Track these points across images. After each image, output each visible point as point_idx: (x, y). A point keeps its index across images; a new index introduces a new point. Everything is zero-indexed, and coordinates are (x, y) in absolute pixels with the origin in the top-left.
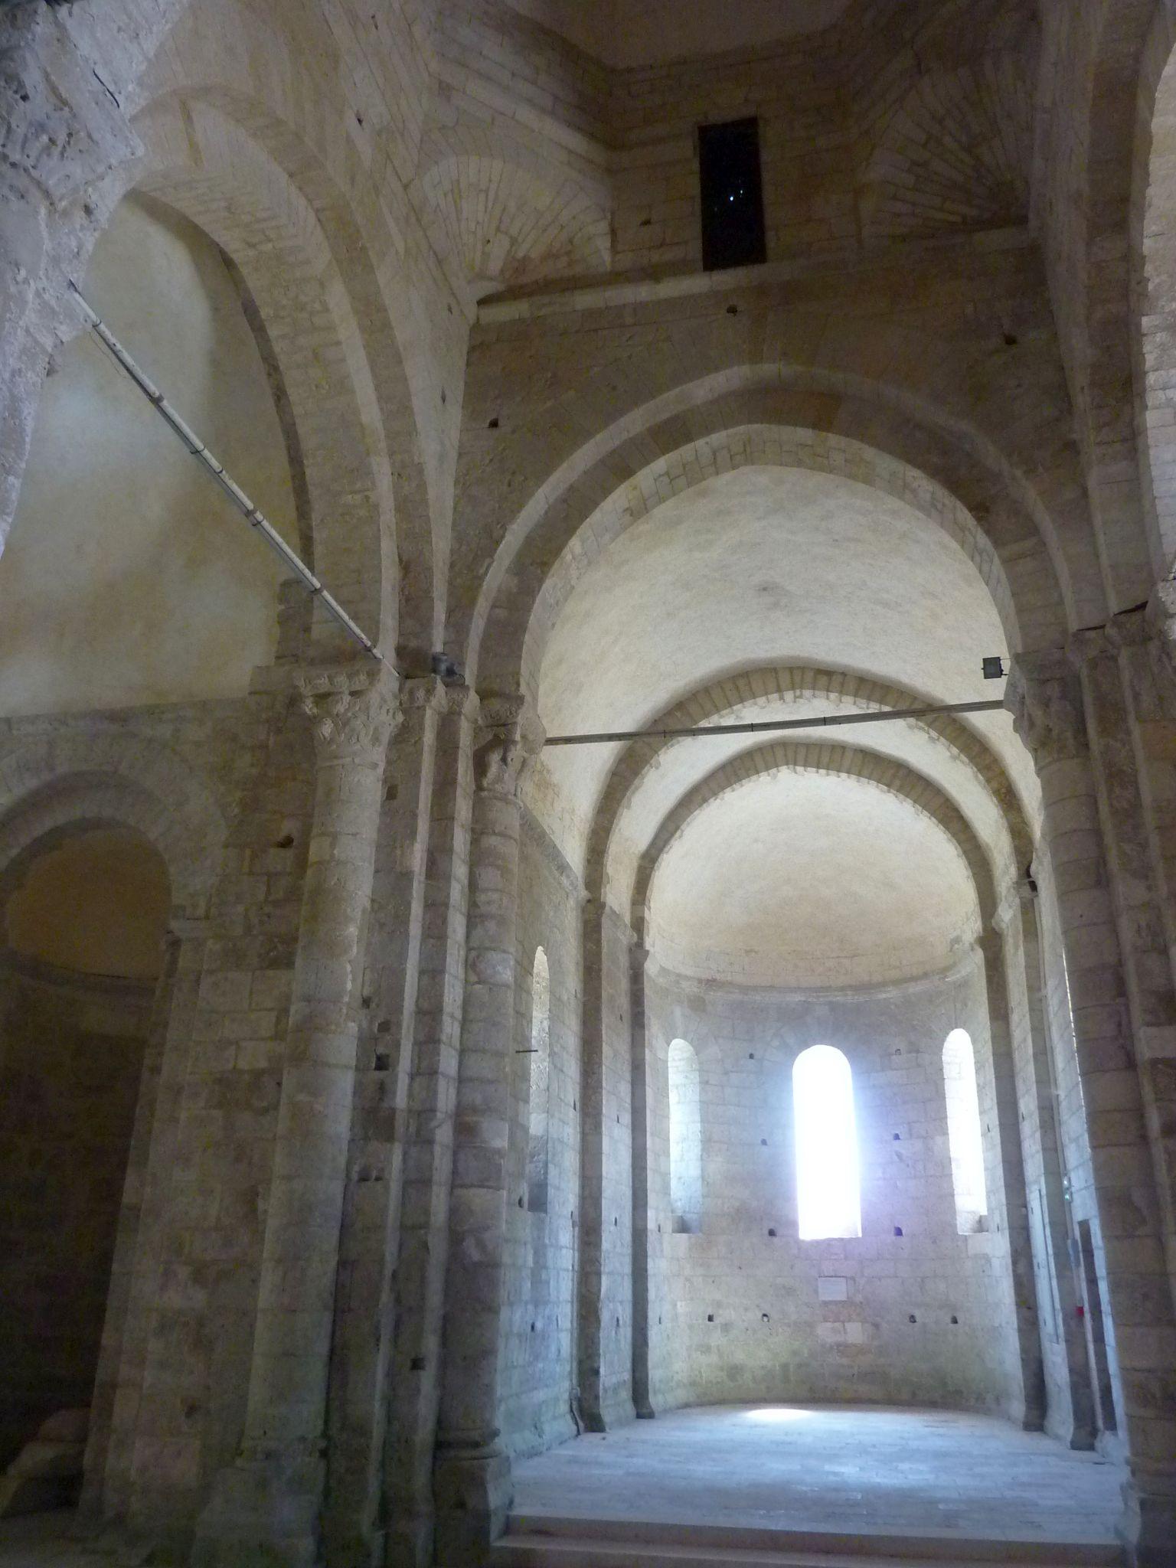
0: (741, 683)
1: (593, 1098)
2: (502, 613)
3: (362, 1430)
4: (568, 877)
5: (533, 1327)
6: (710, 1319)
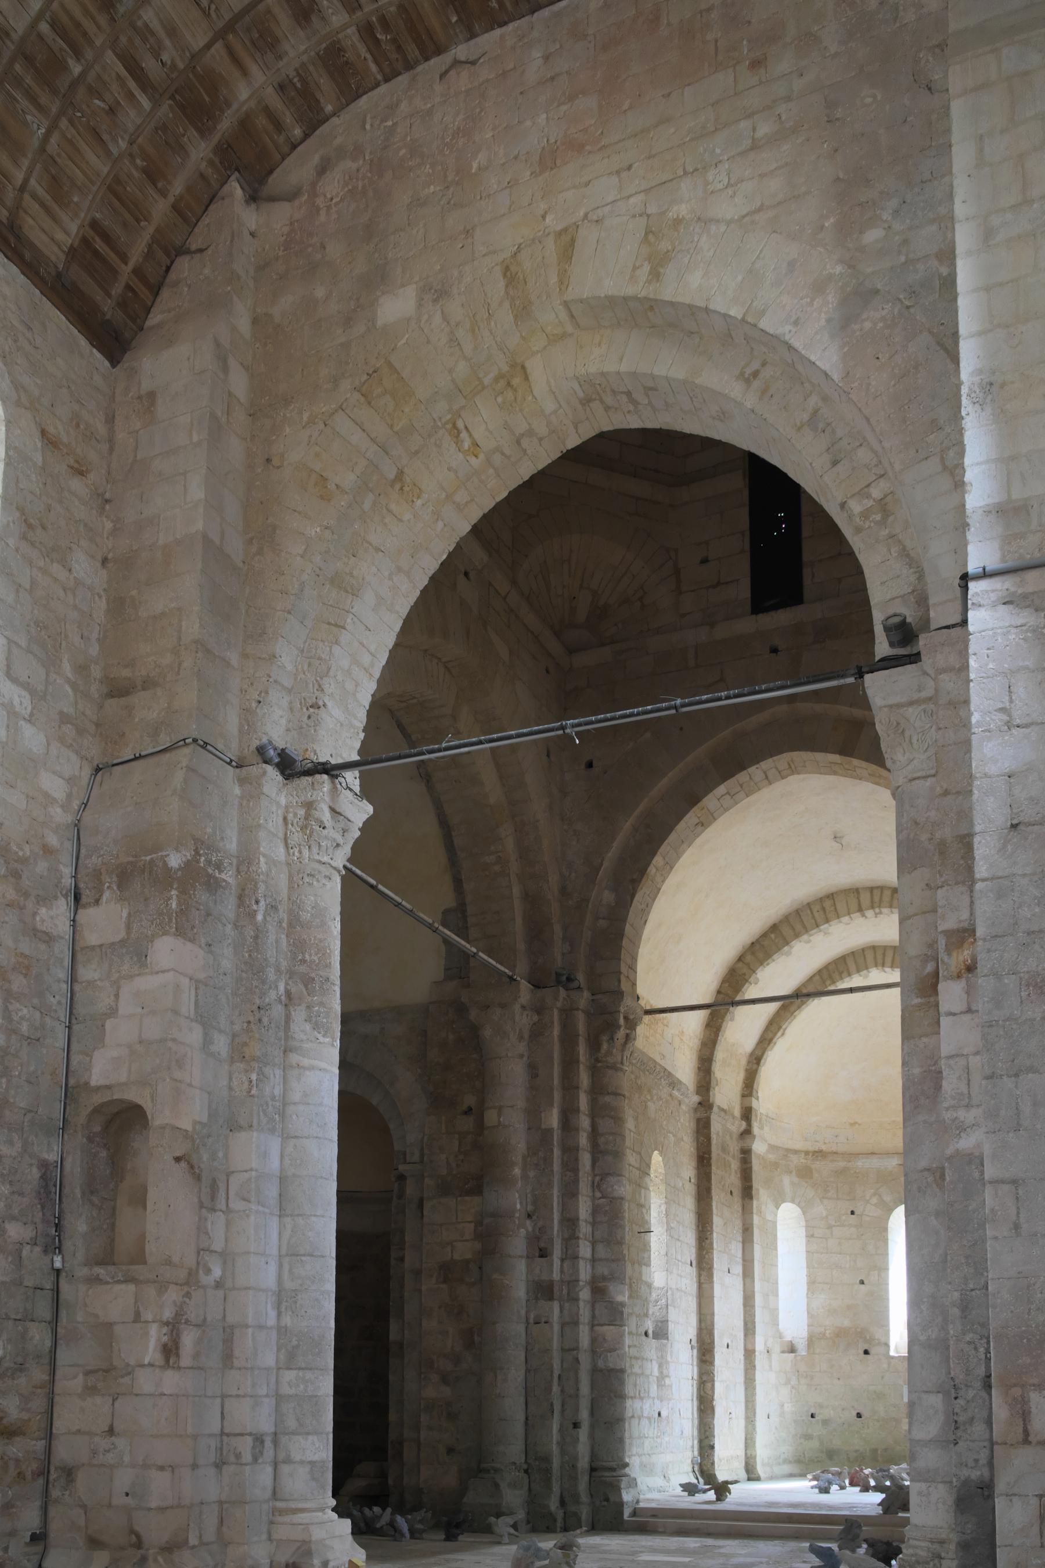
0: (828, 904)
1: (707, 1256)
2: (602, 923)
3: (547, 1459)
4: (679, 1090)
5: (659, 1414)
6: (812, 1416)
